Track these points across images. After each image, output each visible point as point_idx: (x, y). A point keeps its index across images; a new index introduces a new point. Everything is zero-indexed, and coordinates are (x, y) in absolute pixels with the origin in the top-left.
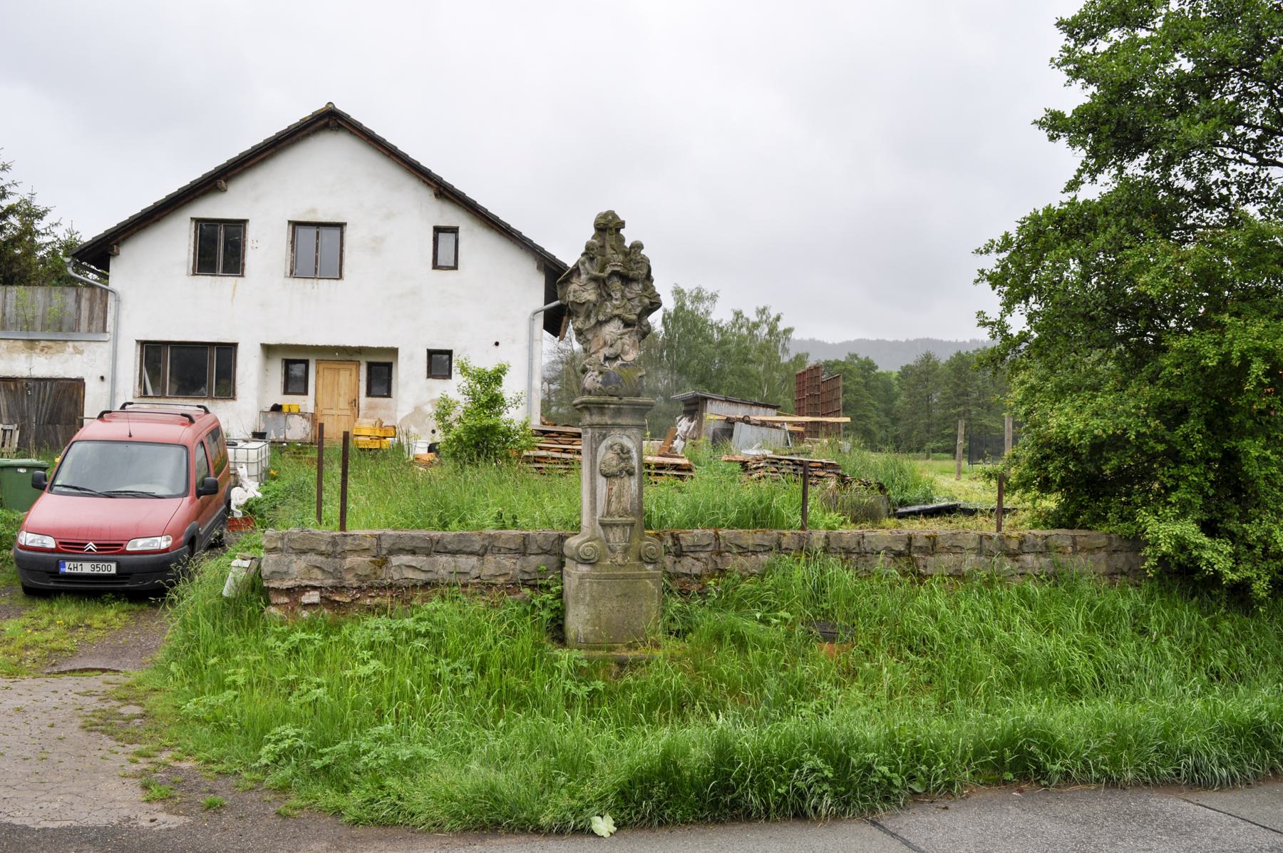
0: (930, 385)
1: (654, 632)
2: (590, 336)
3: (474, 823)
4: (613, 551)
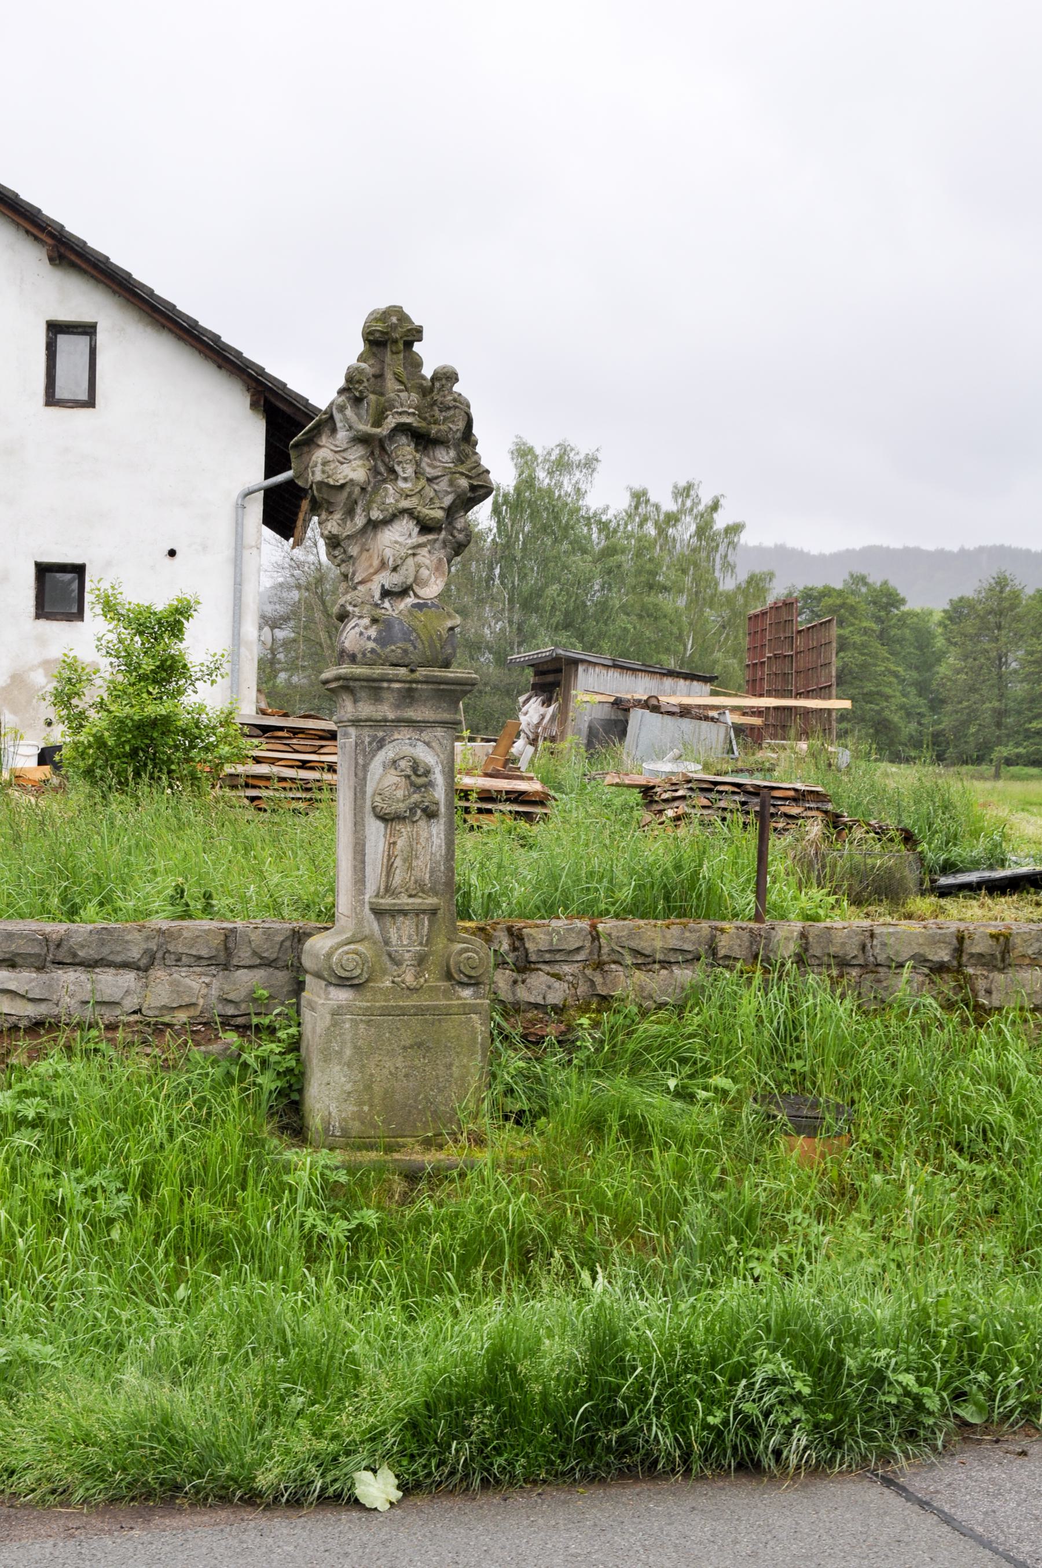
0: (1004, 635)
1: (475, 1116)
2: (354, 550)
3: (130, 1486)
4: (397, 963)
